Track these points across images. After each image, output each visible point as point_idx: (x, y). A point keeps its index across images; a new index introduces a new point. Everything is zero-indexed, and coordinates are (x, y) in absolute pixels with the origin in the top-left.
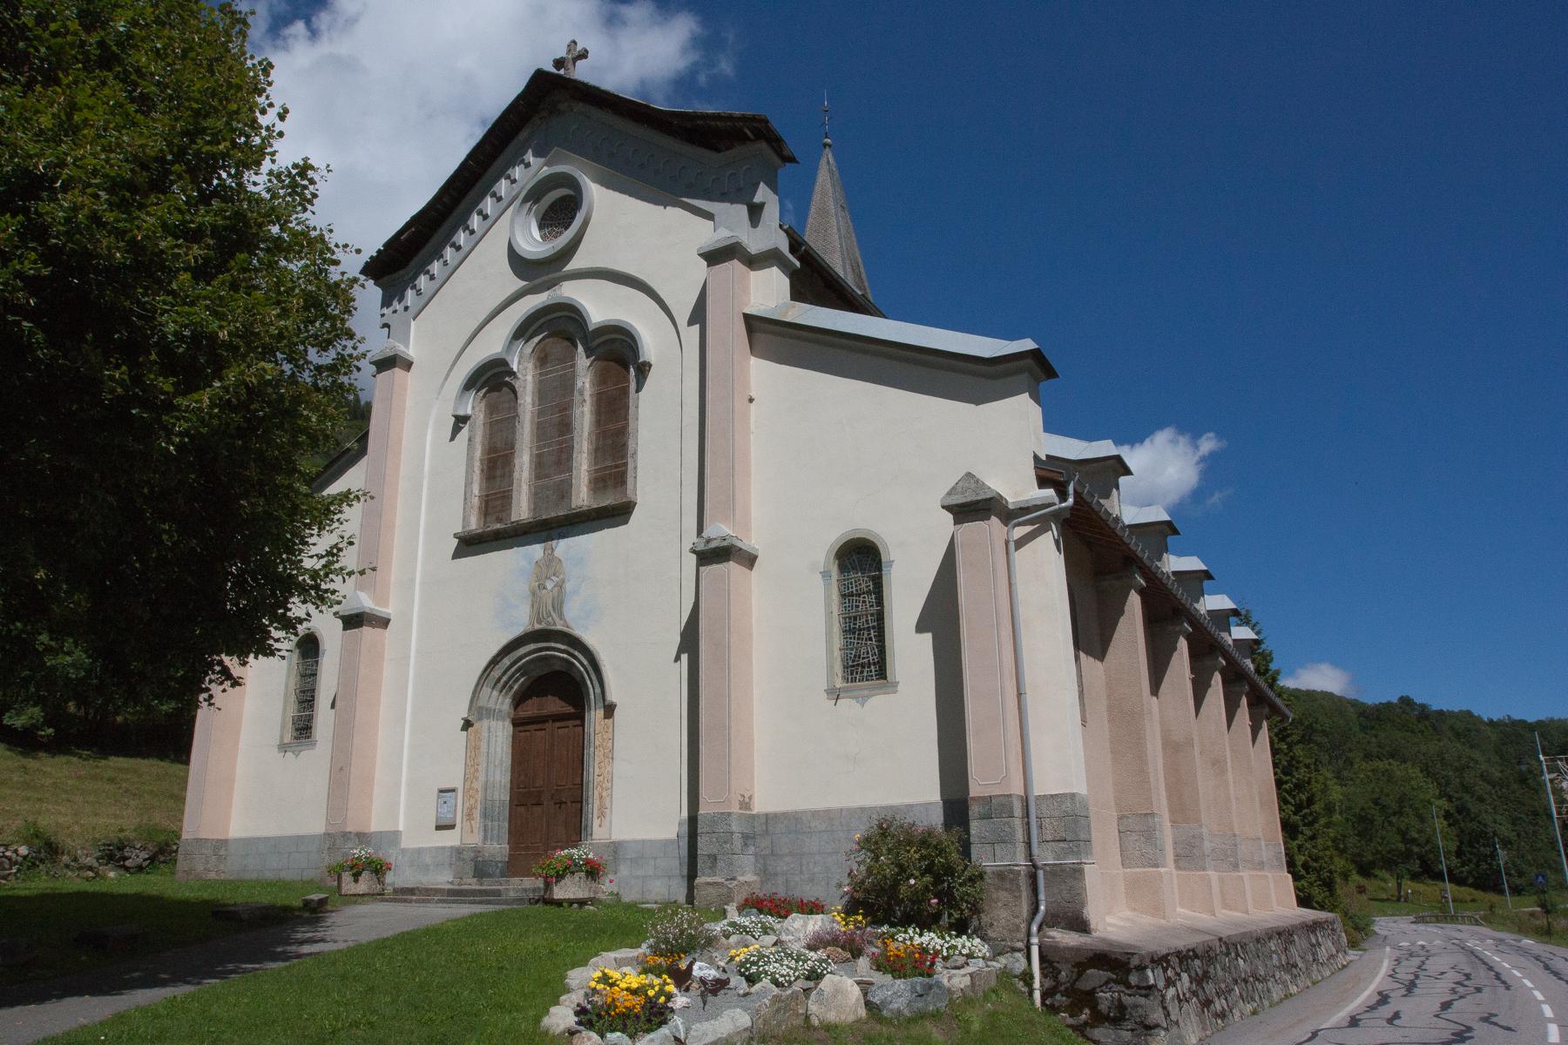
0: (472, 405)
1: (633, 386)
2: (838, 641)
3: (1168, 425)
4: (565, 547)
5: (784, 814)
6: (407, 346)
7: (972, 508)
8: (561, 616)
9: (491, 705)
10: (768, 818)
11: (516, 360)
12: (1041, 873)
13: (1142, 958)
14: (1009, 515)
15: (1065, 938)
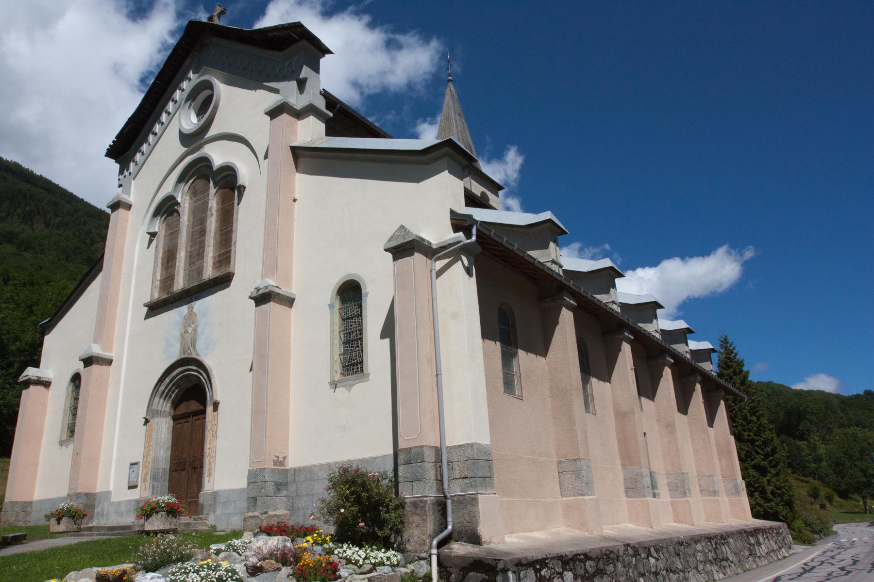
0: (158, 226)
1: (236, 201)
2: (338, 349)
3: (721, 245)
4: (199, 305)
5: (304, 468)
6: (129, 194)
7: (404, 248)
8: (195, 349)
9: (159, 408)
10: (297, 471)
11: (180, 195)
12: (449, 502)
13: (505, 562)
14: (430, 252)
15: (459, 549)
